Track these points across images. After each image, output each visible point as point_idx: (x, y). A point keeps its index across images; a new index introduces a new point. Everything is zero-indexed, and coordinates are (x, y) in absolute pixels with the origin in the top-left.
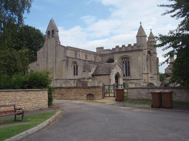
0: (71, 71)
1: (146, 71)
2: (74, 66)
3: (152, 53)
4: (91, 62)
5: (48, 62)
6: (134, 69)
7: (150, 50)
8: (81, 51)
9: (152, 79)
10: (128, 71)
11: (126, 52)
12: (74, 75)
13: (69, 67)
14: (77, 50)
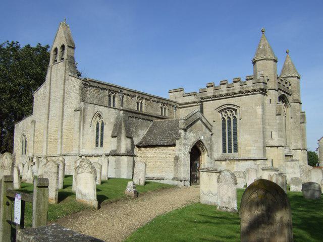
1: (276, 139)
2: (98, 124)
3: (290, 101)
4: (135, 115)
5: (50, 116)
6: (246, 136)
7: (286, 94)
9: (289, 158)
10: (232, 140)
12: (97, 145)
13: (87, 126)
14: (115, 89)
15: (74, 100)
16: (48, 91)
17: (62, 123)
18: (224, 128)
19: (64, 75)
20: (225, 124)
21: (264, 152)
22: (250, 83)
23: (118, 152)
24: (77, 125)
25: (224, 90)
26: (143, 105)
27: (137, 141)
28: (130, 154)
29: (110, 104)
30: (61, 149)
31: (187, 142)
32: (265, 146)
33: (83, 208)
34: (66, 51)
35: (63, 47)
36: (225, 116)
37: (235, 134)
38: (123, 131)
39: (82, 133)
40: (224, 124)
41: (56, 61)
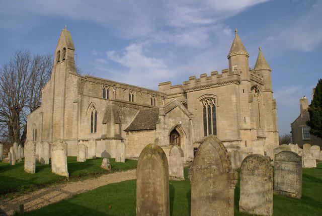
0: (86, 124)
1: (249, 124)
2: (92, 113)
8: (118, 85)
10: (212, 125)
11: (208, 86)
13: (84, 115)
15: (73, 94)
16: (53, 87)
17: (64, 113)
18: (205, 115)
19: (65, 73)
20: (206, 111)
21: (239, 134)
22: (225, 76)
23: (108, 137)
24: (75, 114)
25: (204, 82)
26: (135, 97)
27: (125, 126)
28: (119, 138)
29: (104, 97)
30: (64, 135)
31: (166, 126)
32: (240, 129)
33: (60, 180)
34: (67, 53)
35: (65, 49)
36: (206, 104)
37: (215, 119)
38: (112, 118)
39: (79, 121)
40: (205, 111)
41: (59, 61)
